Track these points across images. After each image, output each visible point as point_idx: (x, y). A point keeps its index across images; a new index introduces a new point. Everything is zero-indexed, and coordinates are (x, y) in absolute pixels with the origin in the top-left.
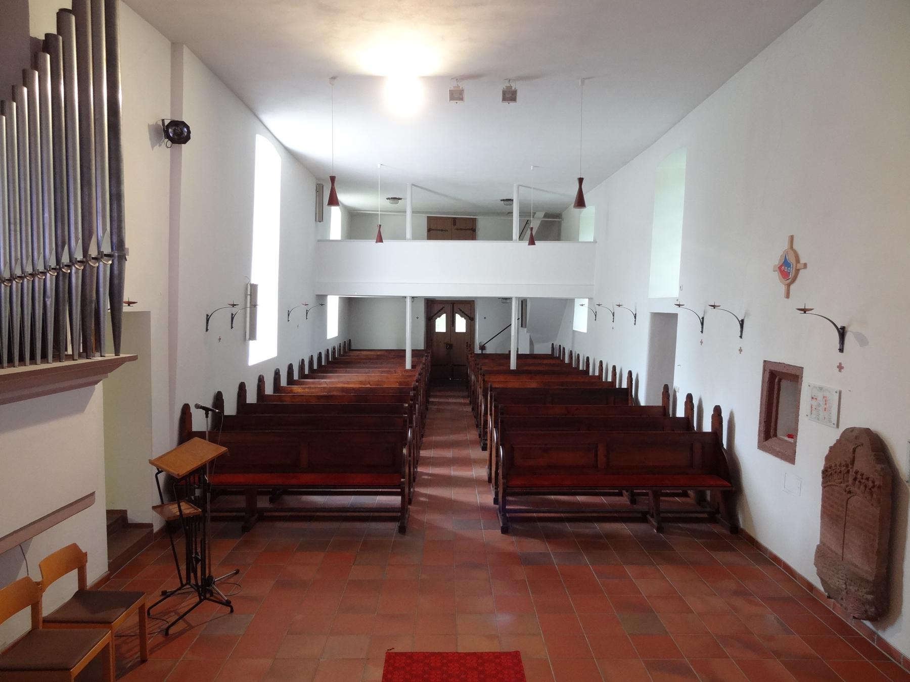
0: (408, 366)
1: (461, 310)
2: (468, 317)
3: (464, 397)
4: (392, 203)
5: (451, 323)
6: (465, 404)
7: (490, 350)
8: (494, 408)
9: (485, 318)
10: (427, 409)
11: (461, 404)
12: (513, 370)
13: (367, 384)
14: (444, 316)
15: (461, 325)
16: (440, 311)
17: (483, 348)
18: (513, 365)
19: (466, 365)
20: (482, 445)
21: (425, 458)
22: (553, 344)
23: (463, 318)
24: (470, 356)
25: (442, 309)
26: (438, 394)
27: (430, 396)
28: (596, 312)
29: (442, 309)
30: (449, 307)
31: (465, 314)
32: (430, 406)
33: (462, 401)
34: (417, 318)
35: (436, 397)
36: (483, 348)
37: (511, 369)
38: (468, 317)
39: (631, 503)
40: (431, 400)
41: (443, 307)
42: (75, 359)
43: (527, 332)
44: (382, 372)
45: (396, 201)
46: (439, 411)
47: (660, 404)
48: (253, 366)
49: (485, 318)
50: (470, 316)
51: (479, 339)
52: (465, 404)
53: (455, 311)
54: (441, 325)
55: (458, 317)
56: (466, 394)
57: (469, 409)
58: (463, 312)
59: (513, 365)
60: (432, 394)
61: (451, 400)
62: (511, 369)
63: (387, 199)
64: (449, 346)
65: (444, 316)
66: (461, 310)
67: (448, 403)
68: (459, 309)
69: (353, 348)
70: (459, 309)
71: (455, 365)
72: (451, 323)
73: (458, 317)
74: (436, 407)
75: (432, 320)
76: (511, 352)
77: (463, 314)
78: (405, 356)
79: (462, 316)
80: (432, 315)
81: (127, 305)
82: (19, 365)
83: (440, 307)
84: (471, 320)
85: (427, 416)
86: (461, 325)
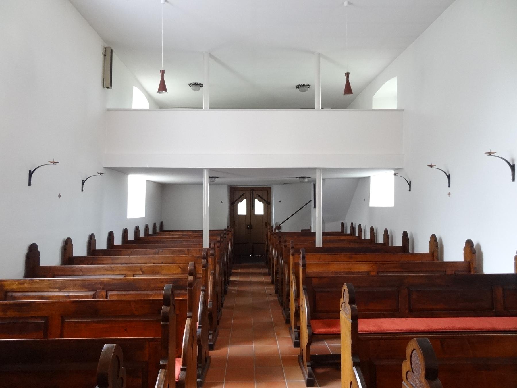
1: (259, 196)
3: (264, 274)
5: (251, 207)
6: (267, 284)
7: (285, 229)
9: (280, 202)
10: (226, 292)
11: (261, 283)
12: (319, 247)
13: (139, 270)
14: (245, 201)
15: (259, 208)
16: (241, 197)
17: (279, 227)
18: (319, 242)
19: (264, 243)
20: (307, 377)
21: (223, 361)
22: (342, 223)
24: (269, 233)
25: (243, 195)
26: (239, 271)
27: (230, 275)
28: (410, 182)
29: (243, 195)
30: (248, 194)
31: (263, 199)
32: (230, 288)
33: (262, 279)
34: (222, 202)
35: (237, 274)
36: (279, 227)
37: (316, 246)
38: (265, 201)
40: (232, 278)
41: (244, 193)
46: (240, 294)
47: (164, 230)
49: (280, 202)
51: (275, 220)
52: (267, 284)
53: (254, 195)
54: (242, 208)
55: (256, 201)
56: (266, 271)
57: (271, 289)
58: (261, 197)
59: (319, 242)
60: (234, 271)
61: (252, 279)
62: (316, 246)
63: (190, 85)
64: (250, 227)
65: (245, 201)
66: (259, 196)
67: (250, 283)
68: (258, 194)
70: (258, 194)
71: (255, 243)
72: (251, 207)
73: (256, 201)
74: (236, 288)
75: (234, 205)
76: (312, 227)
77: (261, 199)
78: (201, 236)
79: (260, 201)
83: (241, 193)
84: (268, 204)
85: (224, 305)
86: (259, 208)
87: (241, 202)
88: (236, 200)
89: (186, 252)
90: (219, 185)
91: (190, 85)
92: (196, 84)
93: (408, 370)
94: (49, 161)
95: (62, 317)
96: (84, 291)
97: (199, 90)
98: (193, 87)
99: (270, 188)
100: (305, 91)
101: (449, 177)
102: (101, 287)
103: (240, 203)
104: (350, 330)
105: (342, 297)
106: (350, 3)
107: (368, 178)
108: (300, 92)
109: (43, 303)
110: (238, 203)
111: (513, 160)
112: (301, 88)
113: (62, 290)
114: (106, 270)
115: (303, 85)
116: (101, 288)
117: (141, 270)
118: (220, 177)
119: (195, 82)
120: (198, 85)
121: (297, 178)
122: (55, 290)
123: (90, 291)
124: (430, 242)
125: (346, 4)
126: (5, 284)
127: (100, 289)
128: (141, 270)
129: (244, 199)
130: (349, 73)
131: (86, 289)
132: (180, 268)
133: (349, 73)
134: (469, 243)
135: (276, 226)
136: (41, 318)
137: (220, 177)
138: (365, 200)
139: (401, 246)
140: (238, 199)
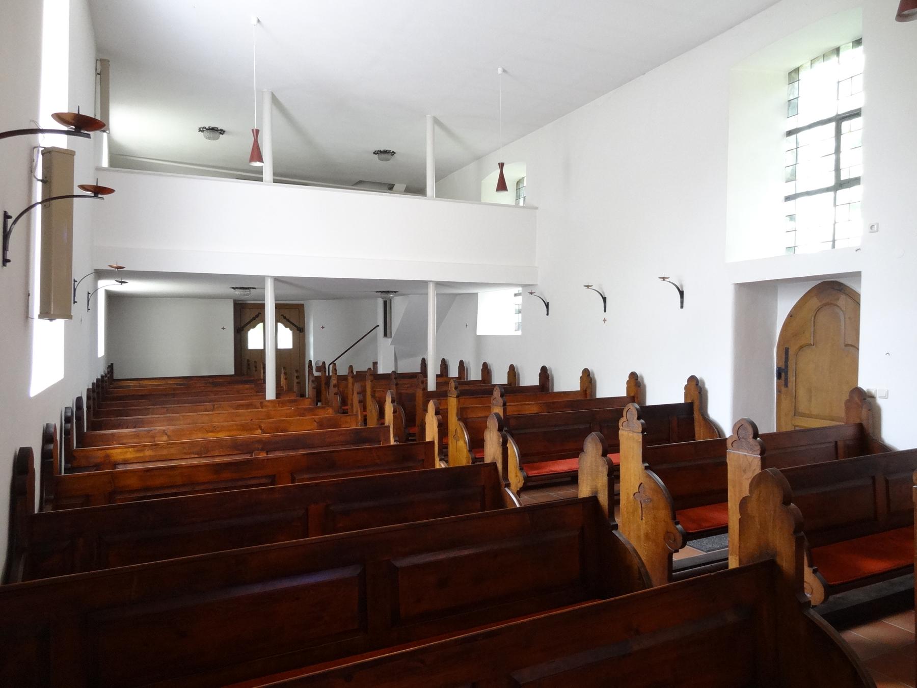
0: (270, 393)
1: (285, 318)
2: (295, 326)
4: (209, 138)
8: (76, 419)
9: (323, 327)
13: (257, 429)
16: (254, 319)
23: (288, 329)
28: (548, 303)
29: (257, 316)
31: (291, 323)
34: (223, 328)
38: (295, 326)
39: (52, 443)
42: (418, 369)
43: (391, 344)
44: (238, 407)
45: (217, 134)
48: (36, 396)
49: (323, 327)
50: (297, 325)
51: (312, 354)
58: (288, 320)
63: (201, 130)
69: (116, 376)
75: (242, 332)
77: (288, 323)
79: (286, 326)
80: (242, 325)
81: (98, 71)
82: (261, 279)
87: (254, 327)
88: (247, 324)
89: (258, 405)
90: (217, 298)
91: (201, 130)
92: (213, 129)
93: (634, 492)
94: (110, 266)
95: (292, 474)
96: (234, 454)
97: (218, 138)
98: (207, 133)
99: (302, 305)
100: (388, 160)
101: (605, 299)
102: (260, 447)
103: (251, 329)
104: (640, 442)
105: (623, 417)
106: (504, 71)
107: (477, 294)
108: (381, 161)
109: (268, 459)
110: (249, 330)
111: (682, 286)
112: (383, 156)
113: (204, 456)
114: (207, 431)
115: (386, 152)
116: (260, 448)
117: (260, 427)
118: (258, 288)
119: (213, 126)
120: (215, 131)
121: (377, 292)
122: (193, 456)
123: (244, 453)
124: (581, 378)
125: (500, 71)
126: (112, 453)
127: (258, 450)
128: (260, 427)
129: (258, 323)
130: (504, 163)
131: (196, 456)
132: (315, 421)
133: (504, 163)
134: (633, 376)
135: (316, 367)
136: (266, 477)
137: (258, 288)
138: (467, 326)
139: (538, 384)
140: (249, 322)
